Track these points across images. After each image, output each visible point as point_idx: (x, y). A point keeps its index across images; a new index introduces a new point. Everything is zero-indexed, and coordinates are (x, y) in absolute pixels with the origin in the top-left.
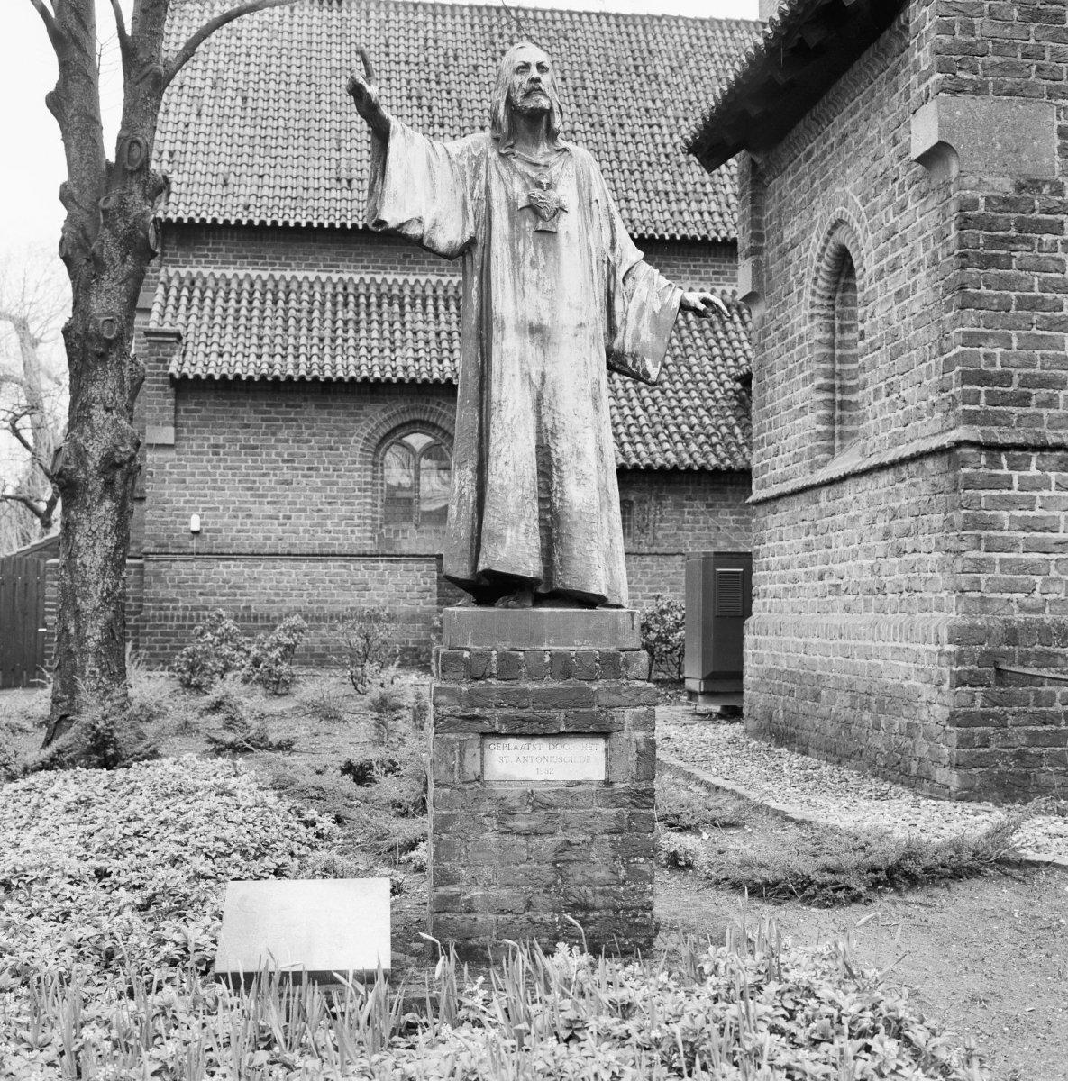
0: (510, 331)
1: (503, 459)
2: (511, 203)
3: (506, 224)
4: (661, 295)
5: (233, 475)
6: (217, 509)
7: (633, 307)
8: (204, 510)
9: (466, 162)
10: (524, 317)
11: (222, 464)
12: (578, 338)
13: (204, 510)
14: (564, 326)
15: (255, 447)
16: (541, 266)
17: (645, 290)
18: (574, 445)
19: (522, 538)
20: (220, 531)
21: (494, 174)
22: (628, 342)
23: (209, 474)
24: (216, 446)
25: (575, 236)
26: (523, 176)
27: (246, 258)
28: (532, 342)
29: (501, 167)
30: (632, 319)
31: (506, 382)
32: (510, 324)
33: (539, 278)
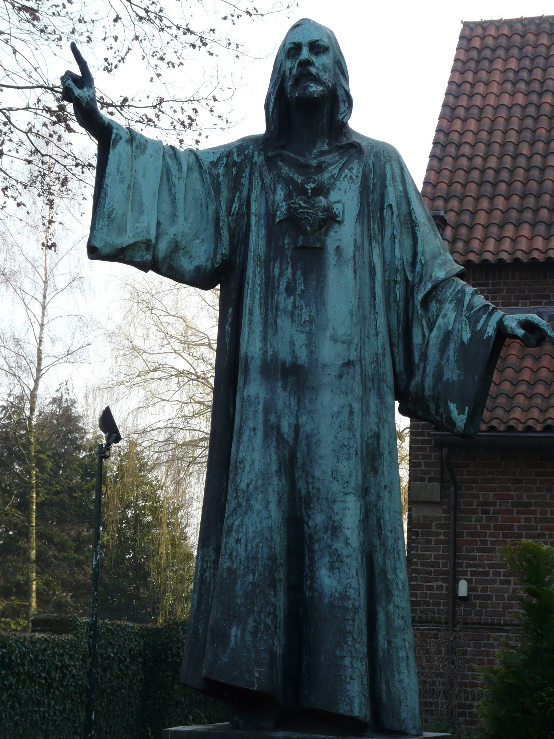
0: (254, 374)
1: (234, 535)
2: (270, 215)
3: (262, 243)
4: (473, 321)
5: (505, 536)
6: (487, 574)
7: (435, 337)
8: (473, 574)
9: (221, 171)
10: (275, 355)
11: (492, 524)
12: (344, 380)
13: (473, 574)
14: (325, 366)
15: (528, 505)
16: (298, 292)
17: (452, 315)
18: (330, 518)
19: (249, 638)
20: (490, 598)
21: (257, 183)
22: (429, 381)
23: (478, 535)
24: (486, 504)
25: (349, 251)
26: (289, 181)
27: (528, 297)
28: (284, 388)
29: (265, 173)
30: (433, 351)
31: (245, 438)
32: (255, 364)
33: (295, 307)
